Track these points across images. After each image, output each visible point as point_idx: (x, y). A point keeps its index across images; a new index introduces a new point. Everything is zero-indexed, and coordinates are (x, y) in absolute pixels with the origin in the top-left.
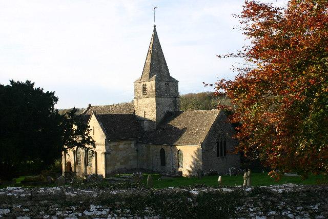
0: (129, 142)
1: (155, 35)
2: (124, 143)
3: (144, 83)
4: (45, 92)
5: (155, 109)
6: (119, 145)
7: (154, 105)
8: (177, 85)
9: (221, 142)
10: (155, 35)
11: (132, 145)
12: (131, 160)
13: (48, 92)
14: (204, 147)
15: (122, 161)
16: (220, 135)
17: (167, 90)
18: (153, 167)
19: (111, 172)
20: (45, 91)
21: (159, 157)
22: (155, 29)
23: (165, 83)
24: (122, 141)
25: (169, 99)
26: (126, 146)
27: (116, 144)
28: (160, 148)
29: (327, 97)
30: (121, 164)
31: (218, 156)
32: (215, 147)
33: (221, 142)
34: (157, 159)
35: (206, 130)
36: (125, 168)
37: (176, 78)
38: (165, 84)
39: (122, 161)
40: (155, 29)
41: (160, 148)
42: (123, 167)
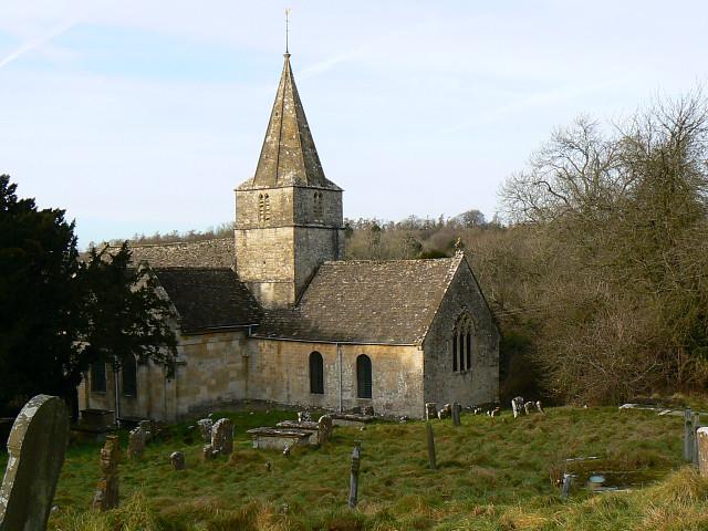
0: (228, 335)
1: (289, 75)
2: (216, 338)
3: (263, 193)
4: (39, 210)
5: (291, 255)
6: (205, 343)
7: (289, 246)
8: (340, 200)
9: (462, 336)
10: (289, 75)
11: (235, 344)
12: (232, 379)
13: (60, 213)
14: (427, 348)
15: (213, 382)
16: (459, 319)
17: (318, 212)
18: (289, 396)
19: (189, 407)
20: (40, 207)
21: (306, 371)
22: (288, 63)
23: (313, 192)
24: (213, 332)
25: (323, 232)
26: (223, 344)
27: (198, 340)
28: (308, 349)
29: (707, 289)
30: (211, 388)
31: (455, 369)
32: (449, 345)
33: (462, 336)
34: (303, 378)
35: (429, 307)
36: (219, 398)
37: (338, 183)
38: (315, 196)
39: (213, 382)
40: (288, 63)
41: (308, 349)
42: (215, 396)
